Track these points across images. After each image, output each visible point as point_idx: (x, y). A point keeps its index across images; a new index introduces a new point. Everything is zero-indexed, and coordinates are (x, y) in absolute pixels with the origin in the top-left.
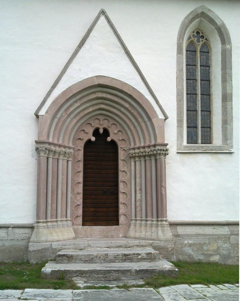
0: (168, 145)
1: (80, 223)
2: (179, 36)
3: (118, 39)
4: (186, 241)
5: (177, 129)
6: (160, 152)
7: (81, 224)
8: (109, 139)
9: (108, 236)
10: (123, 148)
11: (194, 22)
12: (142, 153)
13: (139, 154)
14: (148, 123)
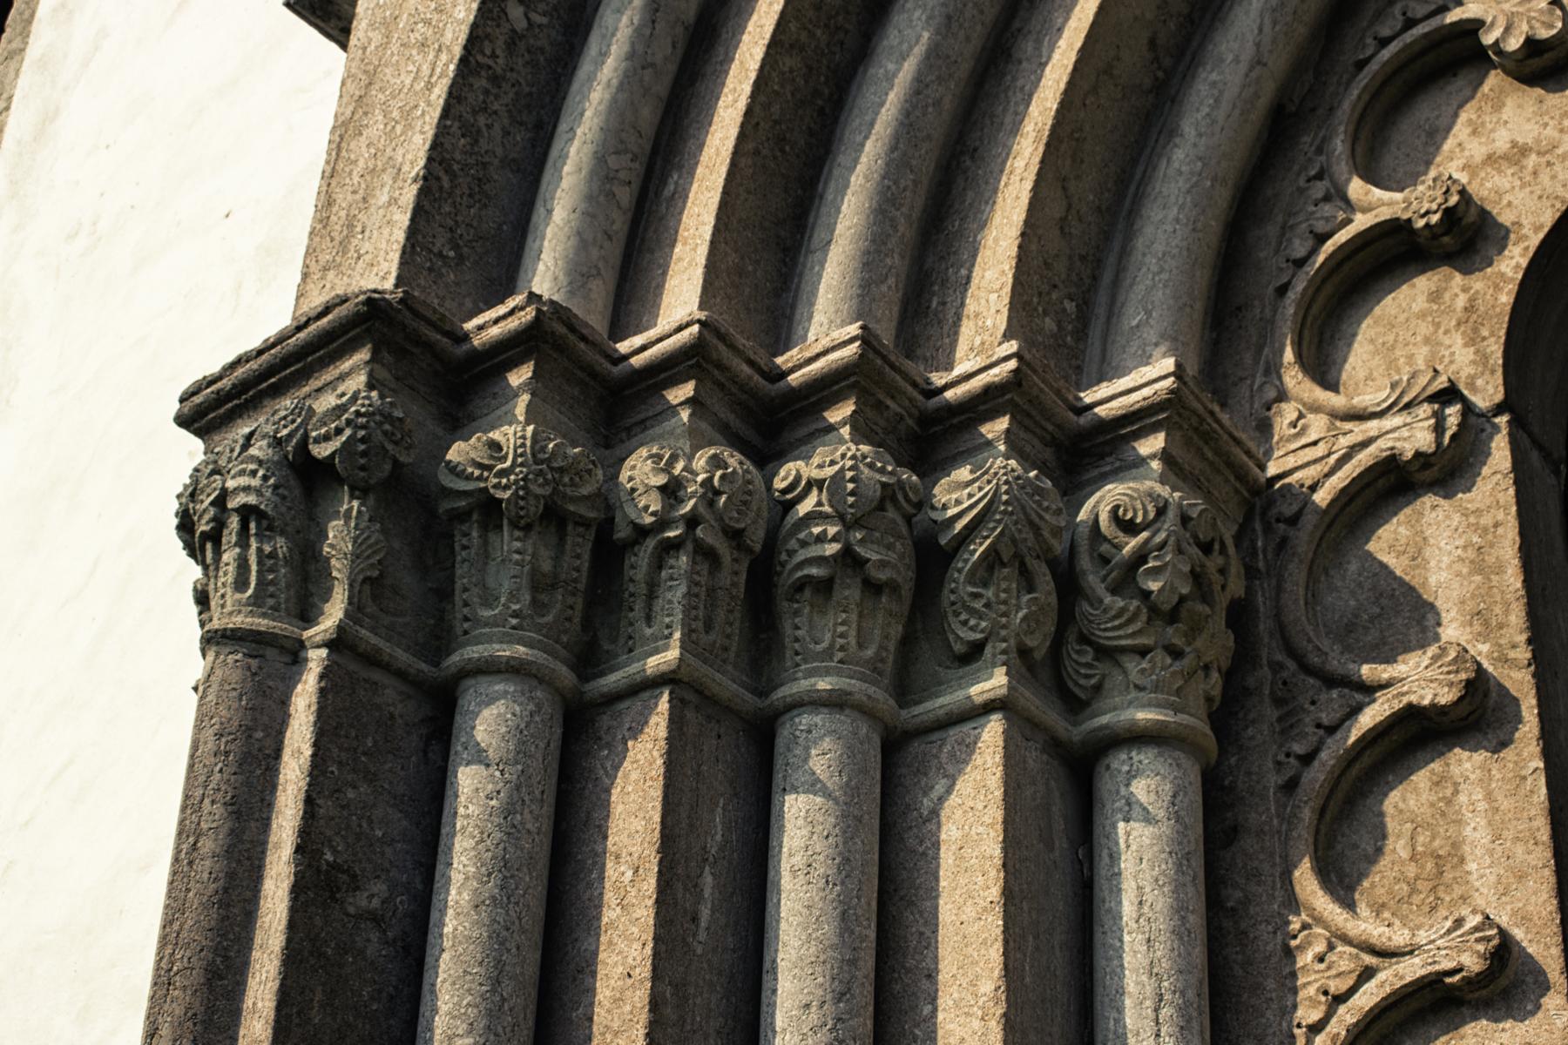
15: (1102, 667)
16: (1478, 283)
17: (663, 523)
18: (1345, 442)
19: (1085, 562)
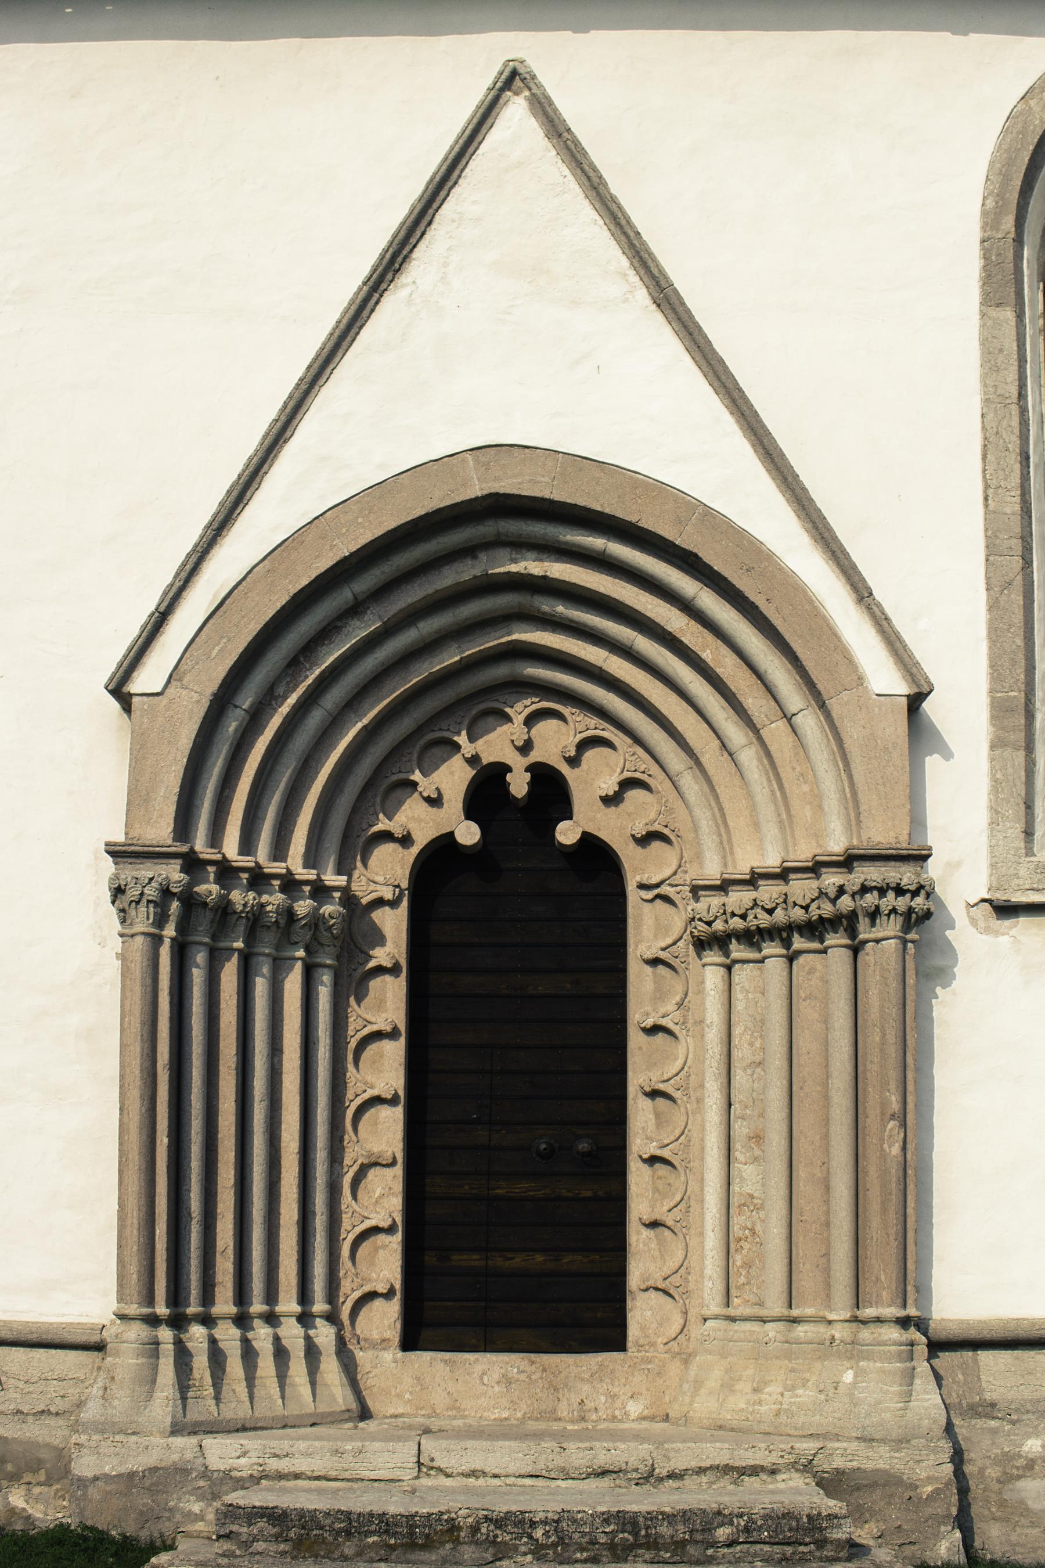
0: (929, 856)
1: (388, 1334)
2: (990, 203)
3: (612, 227)
4: (1030, 1442)
5: (992, 760)
6: (876, 902)
7: (397, 1341)
8: (567, 834)
9: (554, 1410)
10: (658, 885)
11: (1028, 366)
12: (770, 912)
13: (750, 917)
14: (809, 722)
15: (318, 947)
16: (406, 852)
17: (242, 912)
18: (371, 889)
19: (321, 923)
